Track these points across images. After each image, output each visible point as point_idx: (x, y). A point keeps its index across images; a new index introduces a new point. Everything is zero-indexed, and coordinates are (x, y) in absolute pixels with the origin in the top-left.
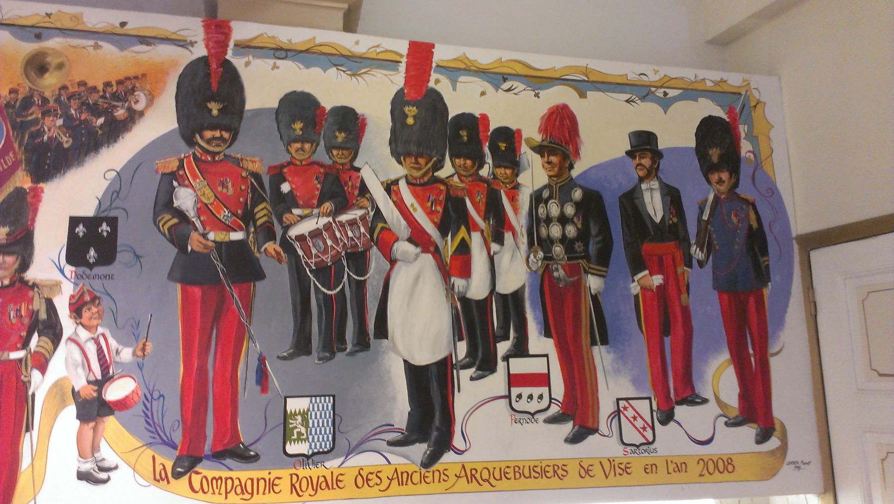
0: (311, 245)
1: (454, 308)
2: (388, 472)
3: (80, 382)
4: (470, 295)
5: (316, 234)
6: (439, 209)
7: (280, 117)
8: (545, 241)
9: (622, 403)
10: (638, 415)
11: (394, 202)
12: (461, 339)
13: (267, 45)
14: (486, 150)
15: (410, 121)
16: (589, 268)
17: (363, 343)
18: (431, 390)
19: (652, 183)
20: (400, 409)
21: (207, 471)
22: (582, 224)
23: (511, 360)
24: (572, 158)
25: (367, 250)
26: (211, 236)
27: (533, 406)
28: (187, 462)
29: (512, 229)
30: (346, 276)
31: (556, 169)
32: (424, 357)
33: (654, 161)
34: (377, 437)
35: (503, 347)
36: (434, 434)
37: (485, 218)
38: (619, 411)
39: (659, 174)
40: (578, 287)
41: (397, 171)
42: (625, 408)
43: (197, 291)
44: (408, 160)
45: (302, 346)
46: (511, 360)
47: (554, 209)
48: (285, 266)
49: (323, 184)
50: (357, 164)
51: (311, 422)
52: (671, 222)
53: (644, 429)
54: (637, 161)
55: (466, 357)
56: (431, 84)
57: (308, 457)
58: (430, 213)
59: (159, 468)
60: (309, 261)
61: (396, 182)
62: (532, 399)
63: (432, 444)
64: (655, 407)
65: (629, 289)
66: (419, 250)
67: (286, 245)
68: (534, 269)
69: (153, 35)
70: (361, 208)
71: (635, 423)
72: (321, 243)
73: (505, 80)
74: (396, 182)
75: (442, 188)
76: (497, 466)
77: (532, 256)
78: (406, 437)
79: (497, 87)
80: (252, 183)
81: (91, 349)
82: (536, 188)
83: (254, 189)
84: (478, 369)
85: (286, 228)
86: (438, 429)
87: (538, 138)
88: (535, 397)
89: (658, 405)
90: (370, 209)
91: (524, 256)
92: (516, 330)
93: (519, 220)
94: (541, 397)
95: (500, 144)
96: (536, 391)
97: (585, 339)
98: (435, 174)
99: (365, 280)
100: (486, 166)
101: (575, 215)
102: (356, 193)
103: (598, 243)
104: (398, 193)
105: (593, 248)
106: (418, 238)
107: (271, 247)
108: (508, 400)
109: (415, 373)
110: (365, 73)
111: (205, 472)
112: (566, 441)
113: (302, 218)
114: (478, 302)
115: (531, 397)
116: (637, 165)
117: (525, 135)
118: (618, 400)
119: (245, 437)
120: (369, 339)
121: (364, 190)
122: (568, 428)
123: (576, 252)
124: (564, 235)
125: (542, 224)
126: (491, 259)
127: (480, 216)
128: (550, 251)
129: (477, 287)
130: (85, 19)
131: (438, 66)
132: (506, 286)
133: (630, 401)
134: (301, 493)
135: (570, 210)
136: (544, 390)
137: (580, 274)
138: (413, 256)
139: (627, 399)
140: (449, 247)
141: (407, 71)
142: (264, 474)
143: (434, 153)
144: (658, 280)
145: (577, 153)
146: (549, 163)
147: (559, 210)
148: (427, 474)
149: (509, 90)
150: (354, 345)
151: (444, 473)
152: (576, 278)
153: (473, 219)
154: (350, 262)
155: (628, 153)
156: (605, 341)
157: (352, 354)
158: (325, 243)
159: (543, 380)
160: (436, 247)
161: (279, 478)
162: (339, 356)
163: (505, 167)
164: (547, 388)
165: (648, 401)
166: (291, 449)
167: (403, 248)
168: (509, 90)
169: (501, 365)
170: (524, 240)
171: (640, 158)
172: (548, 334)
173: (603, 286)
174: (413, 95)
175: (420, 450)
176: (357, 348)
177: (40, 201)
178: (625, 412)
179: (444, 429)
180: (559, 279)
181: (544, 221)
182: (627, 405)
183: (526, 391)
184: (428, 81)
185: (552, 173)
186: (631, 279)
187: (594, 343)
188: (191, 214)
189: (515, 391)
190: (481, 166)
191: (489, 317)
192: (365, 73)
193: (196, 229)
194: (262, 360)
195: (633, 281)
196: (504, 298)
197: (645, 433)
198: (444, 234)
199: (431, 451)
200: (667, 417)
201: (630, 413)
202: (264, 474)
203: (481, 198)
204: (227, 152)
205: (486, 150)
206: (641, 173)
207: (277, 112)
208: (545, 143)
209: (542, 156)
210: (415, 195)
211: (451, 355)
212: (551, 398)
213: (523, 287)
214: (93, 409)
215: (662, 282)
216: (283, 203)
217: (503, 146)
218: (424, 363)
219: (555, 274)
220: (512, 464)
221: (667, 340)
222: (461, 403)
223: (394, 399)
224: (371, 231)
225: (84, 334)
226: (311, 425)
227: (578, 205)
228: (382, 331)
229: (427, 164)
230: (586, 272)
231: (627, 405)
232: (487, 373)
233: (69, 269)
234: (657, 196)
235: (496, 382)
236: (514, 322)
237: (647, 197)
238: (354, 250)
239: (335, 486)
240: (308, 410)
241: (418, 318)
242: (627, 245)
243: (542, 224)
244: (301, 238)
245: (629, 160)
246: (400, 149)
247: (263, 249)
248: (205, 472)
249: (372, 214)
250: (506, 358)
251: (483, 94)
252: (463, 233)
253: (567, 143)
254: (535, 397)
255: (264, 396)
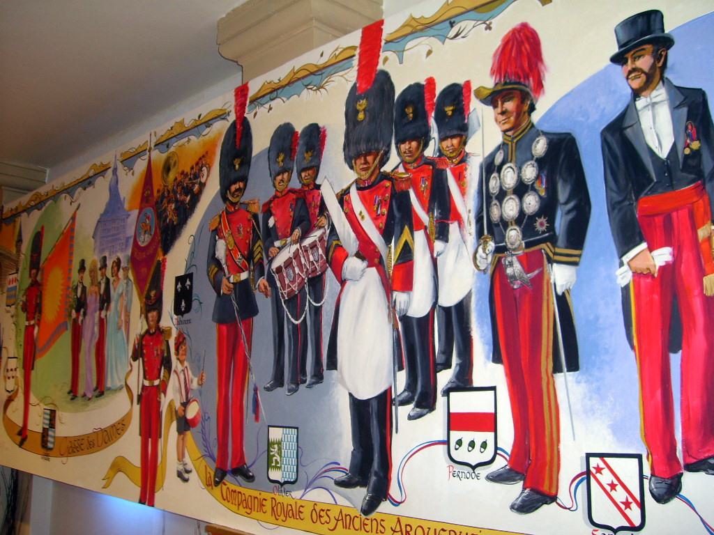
0: (285, 275)
1: (395, 328)
2: (334, 513)
3: (177, 405)
4: (410, 314)
5: (288, 263)
6: (385, 211)
7: (271, 153)
8: (497, 225)
9: (594, 462)
10: (618, 482)
11: (346, 214)
12: (401, 369)
13: (265, 92)
14: (432, 123)
15: (361, 116)
16: (555, 254)
17: (319, 377)
18: (372, 420)
19: (654, 93)
20: (344, 448)
21: (231, 483)
22: (547, 189)
23: (452, 394)
24: (532, 95)
25: (323, 273)
26: (232, 280)
27: (475, 457)
28: (218, 479)
29: (458, 218)
30: (307, 304)
31: (512, 119)
32: (367, 392)
33: (657, 57)
34: (326, 474)
35: (444, 378)
36: (373, 479)
37: (429, 211)
38: (588, 473)
39: (666, 75)
40: (539, 283)
41: (348, 176)
42: (599, 470)
43: (224, 328)
44: (358, 162)
45: (278, 381)
46: (452, 394)
47: (509, 177)
48: (269, 299)
49: (294, 210)
50: (318, 182)
51: (283, 451)
52: (687, 151)
53: (627, 504)
54: (629, 66)
55: (405, 390)
56: (380, 67)
57: (282, 484)
58: (375, 218)
59: (208, 475)
60: (283, 292)
61: (346, 192)
62: (473, 448)
63: (370, 489)
64: (647, 471)
65: (612, 279)
66: (365, 264)
67: (271, 280)
68: (482, 268)
69: (211, 118)
70: (320, 227)
71: (613, 493)
72: (291, 272)
73: (452, 24)
74: (346, 192)
75: (388, 184)
76: (433, 526)
77: (480, 250)
78: (350, 478)
79: (443, 38)
80: (253, 225)
81: (182, 377)
82: (487, 154)
83: (254, 229)
84: (417, 406)
85: (270, 262)
86: (376, 474)
87: (489, 83)
88: (478, 445)
89: (652, 468)
90: (326, 227)
91: (471, 251)
92: (459, 355)
93: (466, 204)
94: (484, 445)
95: (447, 109)
96: (479, 437)
97: (546, 363)
98: (382, 170)
99: (321, 306)
100: (432, 143)
101: (538, 177)
102: (317, 211)
103: (569, 212)
104: (349, 203)
105: (560, 223)
106: (367, 253)
107: (262, 281)
108: (446, 446)
109: (359, 408)
110: (327, 82)
111: (229, 485)
112: (512, 507)
113: (280, 249)
114: (420, 320)
115: (472, 444)
116: (630, 72)
117: (474, 87)
118: (589, 456)
119: (248, 461)
120: (323, 370)
121: (323, 208)
122: (515, 490)
123: (537, 233)
124: (521, 212)
125: (495, 202)
126: (434, 262)
127: (424, 209)
128: (503, 238)
129: (417, 303)
130: (444, 372)
131: (387, 42)
132: (449, 299)
133: (607, 459)
134: (277, 517)
135: (530, 172)
136: (489, 436)
137: (541, 265)
138: (359, 273)
139: (602, 456)
140: (391, 254)
141: (359, 71)
142: (255, 493)
143: (381, 146)
144: (663, 256)
145: (539, 86)
146: (503, 113)
147: (515, 177)
148: (366, 522)
149: (456, 36)
150: (313, 377)
151: (380, 523)
152: (536, 272)
153: (416, 215)
154: (311, 288)
155: (618, 59)
156: (573, 365)
157: (310, 386)
158: (294, 271)
159: (487, 422)
160: (381, 257)
161: (266, 500)
162: (302, 387)
163: (452, 137)
164: (493, 434)
165: (636, 460)
166: (275, 475)
167: (353, 265)
168: (456, 36)
169: (441, 400)
170: (471, 229)
171: (634, 59)
172: (497, 358)
173: (574, 279)
174: (364, 86)
175: (360, 494)
176: (314, 380)
177: (165, 269)
178: (598, 475)
179: (382, 474)
180: (513, 277)
181: (497, 198)
182: (602, 465)
183: (467, 436)
184: (377, 64)
185: (507, 126)
186: (617, 261)
187: (557, 369)
188: (223, 262)
189: (455, 435)
190: (426, 145)
191: (431, 338)
192: (327, 82)
193: (225, 275)
194: (256, 390)
195: (621, 264)
196: (447, 310)
197: (627, 512)
198: (388, 241)
199: (371, 497)
200: (670, 490)
201: (606, 478)
202: (255, 493)
203: (424, 185)
204: (242, 201)
205: (432, 123)
206: (636, 84)
207: (269, 150)
208: (499, 88)
209: (495, 107)
210: (364, 200)
211: (391, 388)
212: (496, 448)
213: (469, 296)
214: (185, 425)
215: (669, 258)
216: (271, 235)
217: (449, 110)
218: (365, 398)
219: (509, 271)
220: (447, 528)
221: (675, 360)
222: (400, 445)
223: (340, 435)
224: (327, 252)
225: (180, 367)
226: (283, 455)
227: (541, 162)
228: (333, 364)
229: (374, 160)
230: (550, 261)
231: (602, 465)
232: (425, 411)
233: (175, 317)
234: (664, 113)
235: (434, 424)
236: (458, 342)
237: (646, 120)
238: (314, 275)
239: (298, 517)
240: (282, 440)
241: (366, 356)
242: (613, 206)
243: (495, 202)
244: (279, 270)
245: (618, 68)
246: (352, 154)
247: (257, 286)
248: (229, 485)
249: (328, 232)
250: (447, 392)
251: (429, 53)
252: (406, 236)
253: (527, 77)
254: (478, 445)
255: (257, 424)
